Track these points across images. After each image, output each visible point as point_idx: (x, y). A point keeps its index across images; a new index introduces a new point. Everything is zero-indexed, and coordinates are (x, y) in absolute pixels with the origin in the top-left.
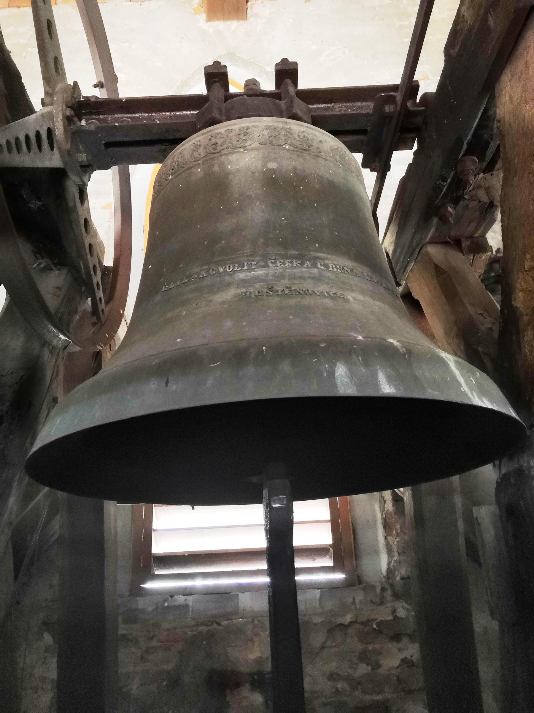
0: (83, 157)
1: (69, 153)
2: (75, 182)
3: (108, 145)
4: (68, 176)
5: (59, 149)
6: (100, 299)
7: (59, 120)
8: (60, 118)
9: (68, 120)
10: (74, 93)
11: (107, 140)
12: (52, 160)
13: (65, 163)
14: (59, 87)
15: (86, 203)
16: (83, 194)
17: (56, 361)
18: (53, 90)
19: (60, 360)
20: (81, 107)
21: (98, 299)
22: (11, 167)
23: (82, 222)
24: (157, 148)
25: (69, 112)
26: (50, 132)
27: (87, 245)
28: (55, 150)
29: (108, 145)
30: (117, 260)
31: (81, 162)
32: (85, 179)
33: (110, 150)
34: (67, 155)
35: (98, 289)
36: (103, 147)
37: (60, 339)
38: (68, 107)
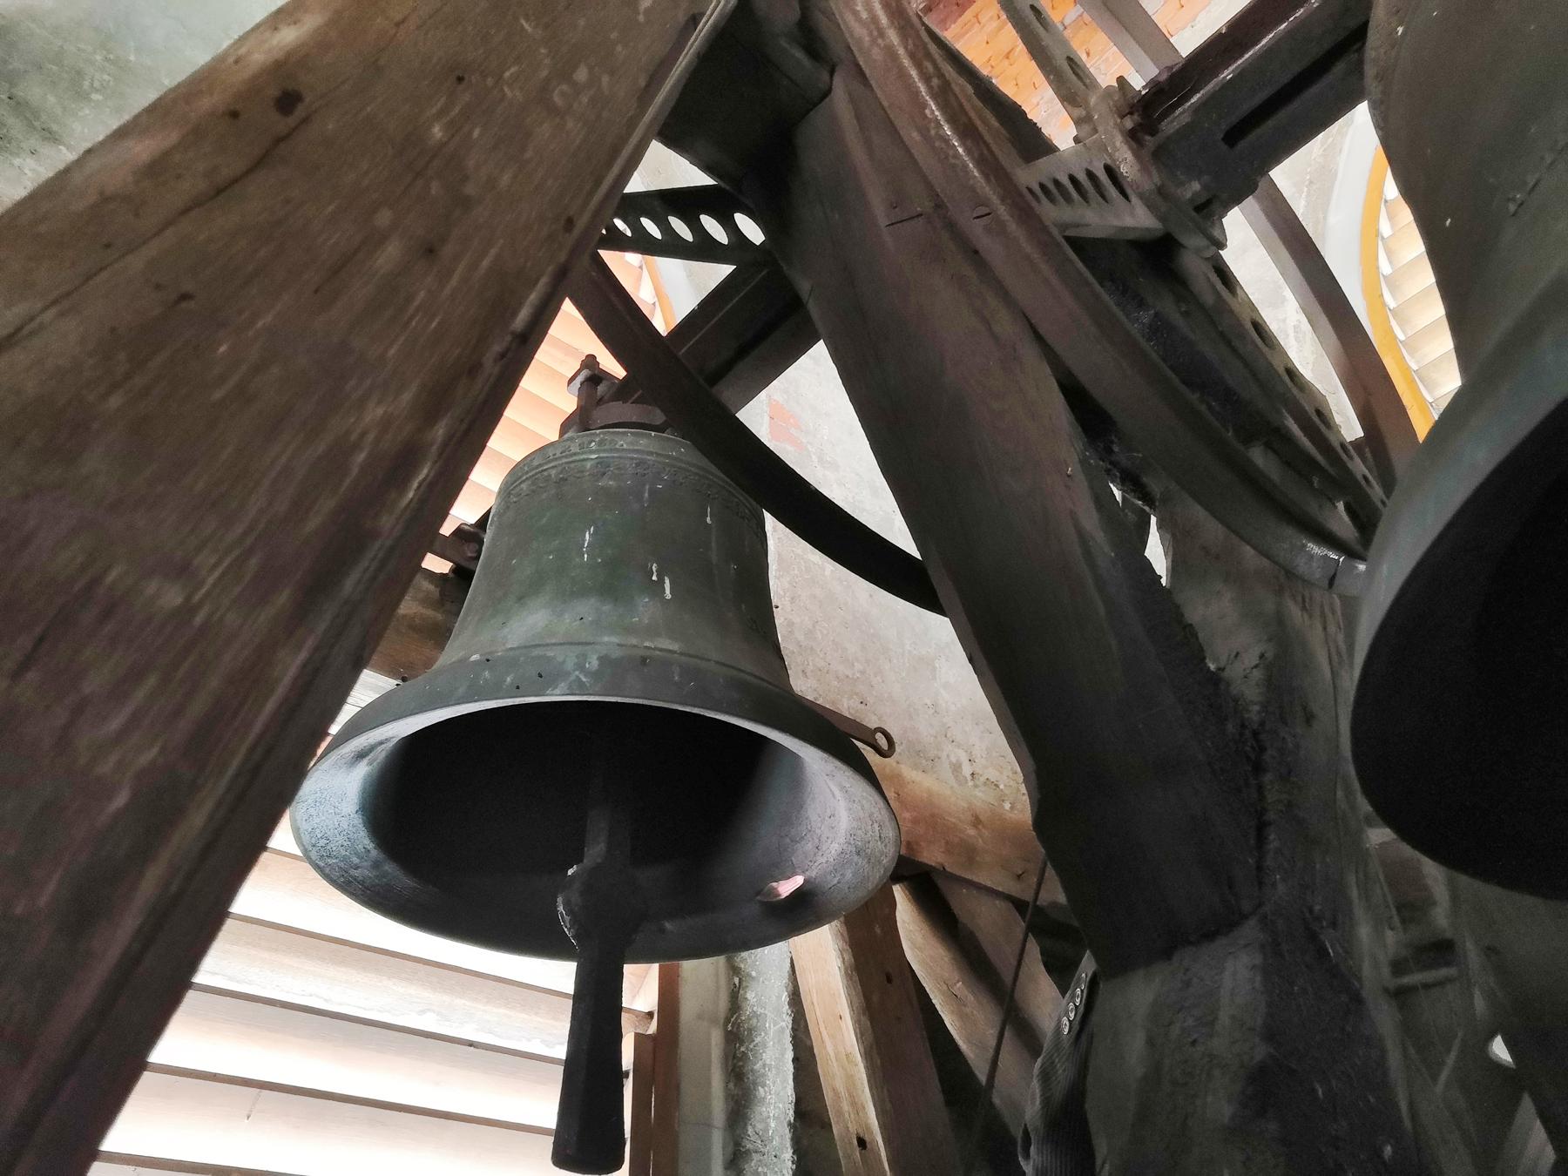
0: (1194, 188)
1: (1160, 191)
2: (1198, 251)
3: (1234, 136)
4: (1181, 245)
5: (1141, 196)
6: (1365, 477)
7: (1118, 144)
8: (1119, 140)
9: (1133, 136)
10: (1124, 94)
11: (1224, 127)
12: (1138, 218)
13: (1162, 218)
14: (1093, 100)
15: (1239, 291)
16: (1224, 275)
17: (1325, 628)
18: (1087, 107)
19: (1332, 629)
20: (1146, 112)
21: (1359, 477)
22: (1077, 419)
23: (1249, 326)
24: (1339, 68)
25: (1129, 123)
26: (1110, 171)
27: (1281, 370)
28: (1134, 199)
29: (1234, 136)
30: (1366, 416)
31: (1192, 200)
32: (1216, 233)
33: (1243, 145)
34: (1159, 199)
35: (1351, 458)
36: (1224, 147)
37: (1312, 557)
38: (1122, 117)
